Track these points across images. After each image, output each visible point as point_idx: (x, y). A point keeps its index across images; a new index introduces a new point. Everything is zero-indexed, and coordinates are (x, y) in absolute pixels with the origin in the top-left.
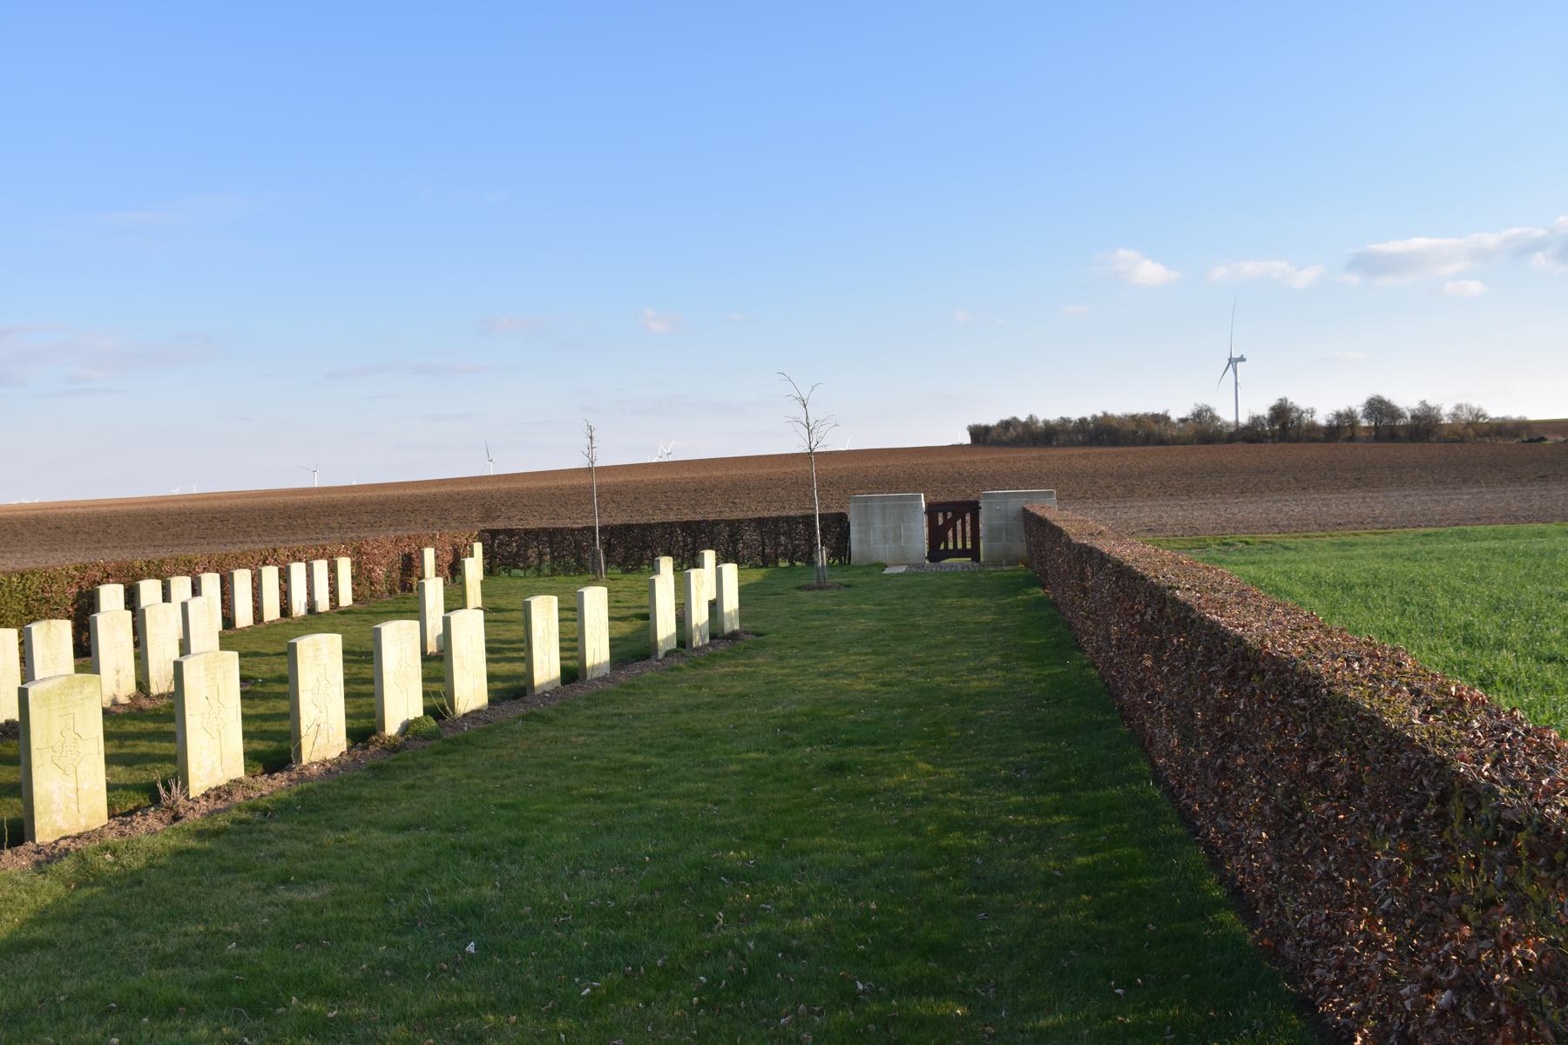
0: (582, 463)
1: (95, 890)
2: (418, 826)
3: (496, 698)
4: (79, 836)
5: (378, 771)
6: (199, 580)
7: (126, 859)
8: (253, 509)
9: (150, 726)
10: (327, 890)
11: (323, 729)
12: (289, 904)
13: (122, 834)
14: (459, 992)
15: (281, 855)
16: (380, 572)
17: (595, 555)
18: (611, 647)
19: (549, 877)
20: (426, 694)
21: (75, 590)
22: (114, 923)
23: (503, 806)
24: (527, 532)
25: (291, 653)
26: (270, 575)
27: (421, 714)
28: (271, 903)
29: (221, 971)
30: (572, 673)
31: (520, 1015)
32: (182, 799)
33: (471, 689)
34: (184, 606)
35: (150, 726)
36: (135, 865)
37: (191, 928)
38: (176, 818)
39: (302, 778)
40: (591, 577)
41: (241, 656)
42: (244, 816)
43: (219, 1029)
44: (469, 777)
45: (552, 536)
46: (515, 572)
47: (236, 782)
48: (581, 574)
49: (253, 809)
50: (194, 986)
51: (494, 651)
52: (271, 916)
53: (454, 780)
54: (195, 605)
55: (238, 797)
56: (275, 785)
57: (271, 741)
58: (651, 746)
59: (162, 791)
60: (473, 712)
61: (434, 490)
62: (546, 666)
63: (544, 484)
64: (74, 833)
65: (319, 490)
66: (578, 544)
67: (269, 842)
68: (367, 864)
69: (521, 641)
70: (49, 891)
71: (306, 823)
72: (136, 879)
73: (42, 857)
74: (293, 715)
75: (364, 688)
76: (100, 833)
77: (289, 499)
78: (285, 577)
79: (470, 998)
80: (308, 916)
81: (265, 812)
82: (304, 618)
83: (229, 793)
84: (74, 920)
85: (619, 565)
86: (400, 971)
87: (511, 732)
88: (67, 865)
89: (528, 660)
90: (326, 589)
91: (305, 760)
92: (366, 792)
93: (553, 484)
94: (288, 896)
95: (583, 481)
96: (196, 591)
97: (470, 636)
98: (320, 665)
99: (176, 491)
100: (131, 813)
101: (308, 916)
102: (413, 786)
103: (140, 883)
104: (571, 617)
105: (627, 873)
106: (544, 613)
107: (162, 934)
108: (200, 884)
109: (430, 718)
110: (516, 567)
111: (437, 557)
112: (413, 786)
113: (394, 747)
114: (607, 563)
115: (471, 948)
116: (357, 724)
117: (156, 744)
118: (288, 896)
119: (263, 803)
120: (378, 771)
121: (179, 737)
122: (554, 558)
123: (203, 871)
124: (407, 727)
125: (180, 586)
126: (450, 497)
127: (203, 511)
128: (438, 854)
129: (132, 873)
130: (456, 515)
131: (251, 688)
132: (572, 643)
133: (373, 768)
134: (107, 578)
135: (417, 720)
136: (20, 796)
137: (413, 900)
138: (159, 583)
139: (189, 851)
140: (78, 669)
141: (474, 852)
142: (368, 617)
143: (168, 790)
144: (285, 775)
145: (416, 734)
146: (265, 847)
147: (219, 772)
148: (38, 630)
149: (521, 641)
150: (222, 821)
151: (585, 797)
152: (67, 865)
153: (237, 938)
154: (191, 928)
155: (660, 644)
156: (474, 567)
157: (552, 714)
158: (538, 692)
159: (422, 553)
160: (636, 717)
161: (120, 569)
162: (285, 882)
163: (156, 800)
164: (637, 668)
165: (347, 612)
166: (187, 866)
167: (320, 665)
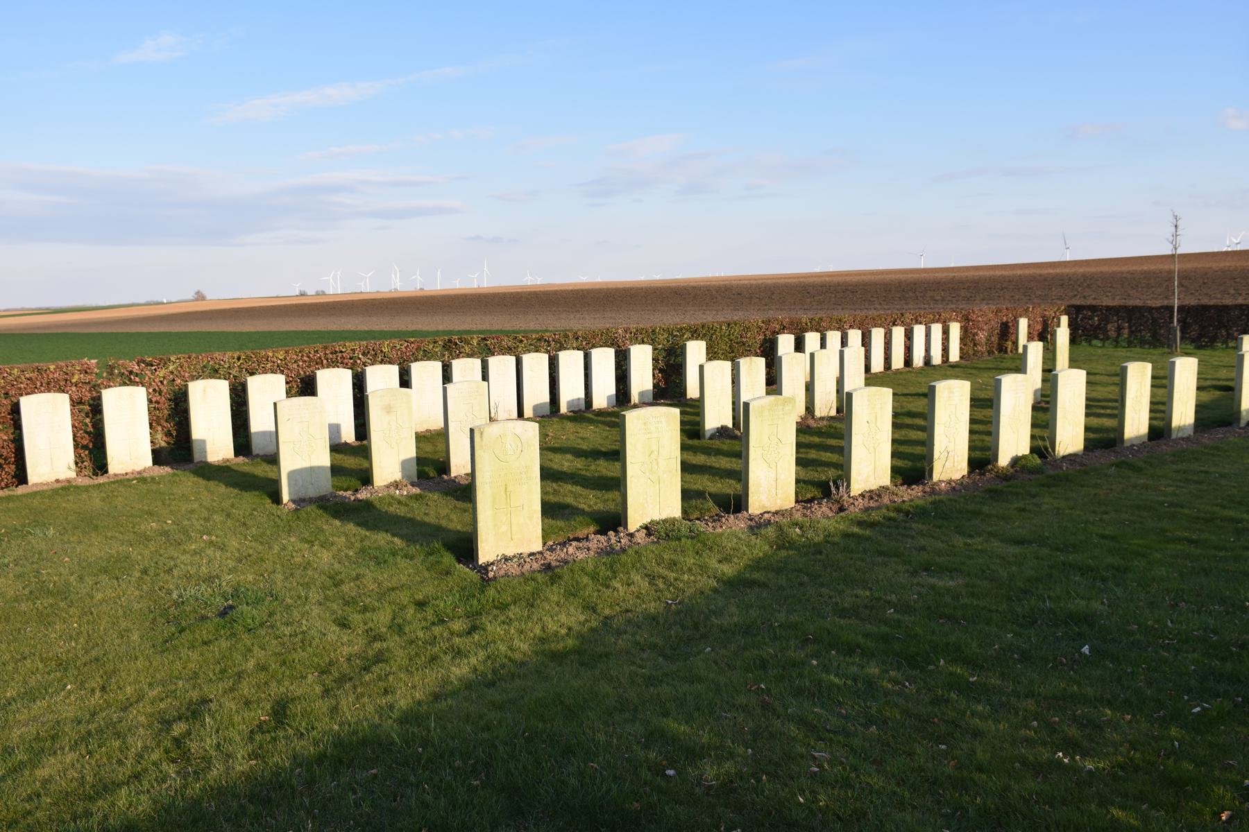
0: (1166, 250)
1: (791, 552)
2: (1030, 542)
3: (1090, 445)
4: (777, 513)
5: (994, 494)
6: (891, 331)
7: (810, 534)
8: (875, 284)
9: (816, 440)
10: (960, 582)
11: (950, 457)
12: (933, 587)
13: (805, 515)
14: (1079, 684)
15: (922, 548)
16: (982, 336)
17: (1171, 331)
18: (1196, 412)
19: (1152, 603)
20: (1033, 437)
21: (762, 337)
22: (806, 579)
23: (1104, 537)
24: (1108, 308)
25: (930, 395)
26: (898, 333)
27: (1027, 452)
28: (918, 584)
29: (884, 629)
30: (1160, 429)
31: (1134, 716)
32: (845, 497)
33: (1070, 436)
34: (812, 355)
35: (816, 440)
36: (817, 539)
37: (860, 592)
38: (841, 509)
39: (933, 492)
40: (1166, 350)
41: (1088, 374)
42: (892, 514)
43: (887, 671)
44: (1072, 509)
45: (1131, 314)
46: (1095, 342)
47: (884, 488)
48: (1155, 347)
49: (898, 510)
50: (867, 636)
51: (1092, 406)
52: (919, 594)
53: (1058, 509)
54: (821, 356)
55: (886, 500)
56: (911, 495)
57: (912, 460)
58: (1240, 503)
59: (833, 489)
60: (1070, 455)
61: (1019, 272)
62: (1136, 423)
63: (1116, 269)
64: (773, 510)
65: (925, 270)
66: (1155, 321)
67: (913, 537)
68: (992, 566)
69: (1116, 401)
70: (760, 548)
71: (940, 527)
72: (817, 549)
73: (753, 524)
74: (929, 443)
75: (1161, 407)
76: (790, 512)
77: (902, 277)
78: (909, 336)
79: (1089, 691)
80: (948, 599)
81: (907, 513)
82: (921, 368)
83: (879, 496)
84: (778, 571)
85: (1193, 341)
86: (1026, 657)
87: (1106, 475)
88: (770, 531)
89: (1120, 416)
90: (940, 347)
91: (936, 477)
92: (986, 509)
93: (1125, 269)
94: (932, 580)
95: (1166, 267)
96: (823, 345)
97: (1073, 388)
98: (952, 403)
99: (818, 270)
100: (810, 501)
101: (948, 599)
102: (1023, 510)
103: (821, 553)
104: (1163, 384)
105: (1227, 613)
106: (1139, 376)
107: (840, 593)
108: (863, 560)
109: (1036, 456)
110: (1096, 338)
111: (1029, 326)
112: (1023, 510)
113: (1004, 476)
114: (1182, 339)
115: (1086, 649)
116: (978, 454)
117: (823, 453)
118: (932, 580)
119: (905, 507)
120: (994, 494)
121: (846, 450)
122: (1131, 333)
123: (865, 551)
124: (1016, 461)
125: (834, 337)
126: (1033, 278)
127: (839, 284)
128: (1051, 567)
129: (815, 544)
130: (1039, 293)
131: (900, 420)
132: (1161, 406)
133: (989, 491)
134: (783, 329)
135: (1024, 457)
136: (740, 480)
137: (1033, 602)
138: (818, 335)
139: (853, 535)
140: (768, 393)
141: (1084, 570)
142: (973, 371)
143: (837, 488)
144: (921, 488)
145: (1023, 467)
146: (910, 540)
147: (872, 479)
148: (744, 363)
149: (1116, 401)
150: (875, 516)
151: (1180, 540)
152: (770, 531)
153: (895, 607)
154: (860, 592)
155: (1244, 414)
156: (1063, 334)
157: (1141, 464)
158: (1127, 444)
159: (1017, 323)
160: (1223, 476)
161: (792, 323)
162: (926, 570)
163: (827, 494)
164: (1220, 433)
165: (954, 366)
166: (853, 546)
167: (952, 403)
